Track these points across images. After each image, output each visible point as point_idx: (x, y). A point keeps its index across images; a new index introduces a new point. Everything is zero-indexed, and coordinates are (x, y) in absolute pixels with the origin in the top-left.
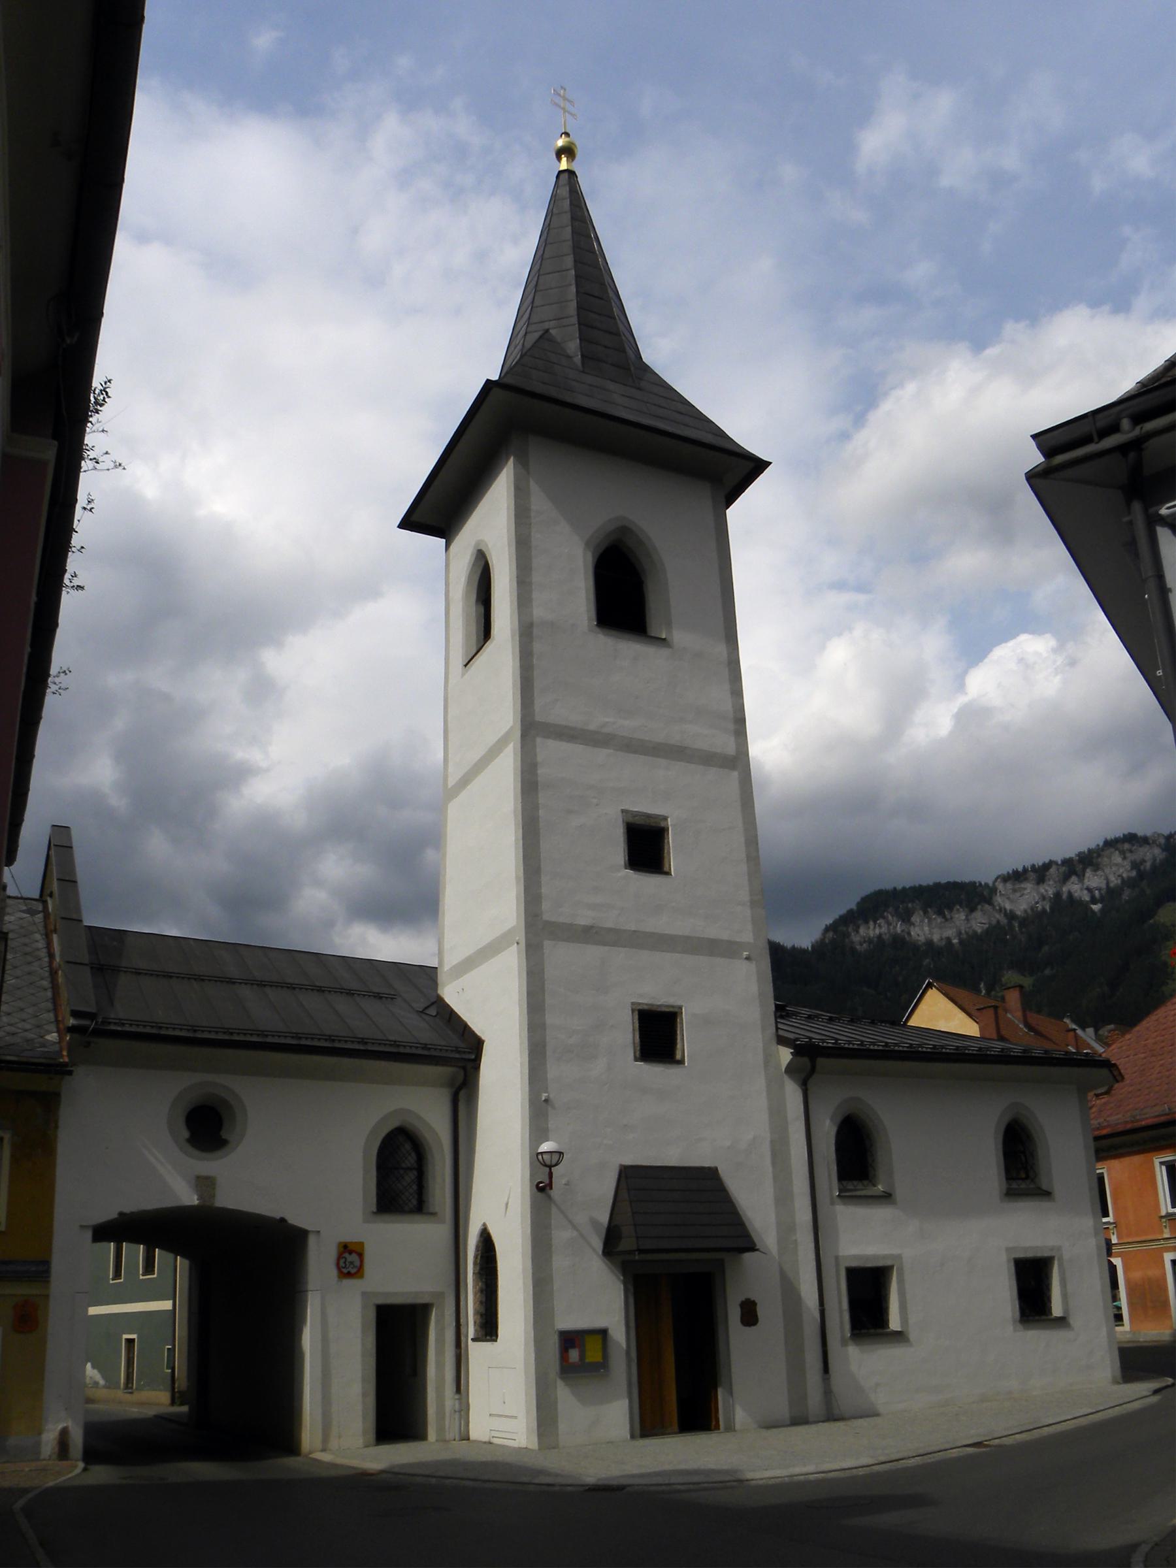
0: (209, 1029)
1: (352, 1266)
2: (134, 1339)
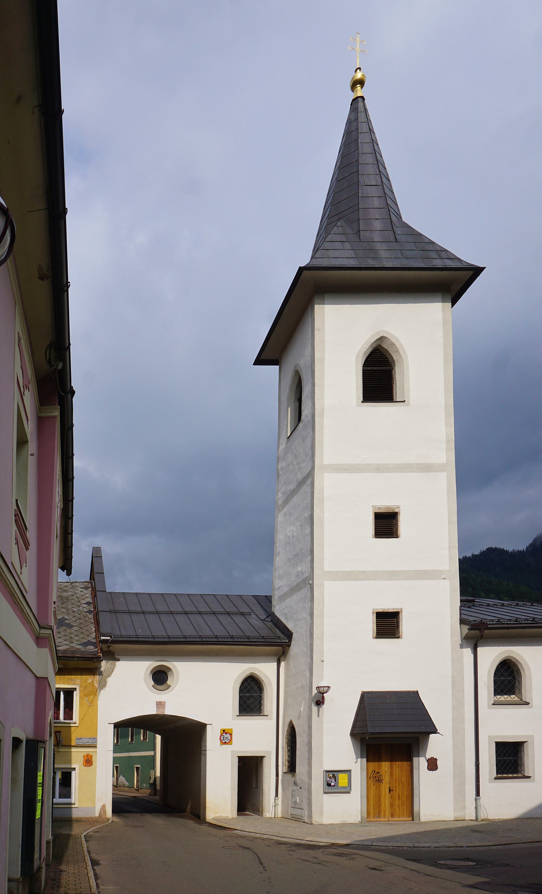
0: (218, 612)
1: (227, 739)
2: (139, 767)
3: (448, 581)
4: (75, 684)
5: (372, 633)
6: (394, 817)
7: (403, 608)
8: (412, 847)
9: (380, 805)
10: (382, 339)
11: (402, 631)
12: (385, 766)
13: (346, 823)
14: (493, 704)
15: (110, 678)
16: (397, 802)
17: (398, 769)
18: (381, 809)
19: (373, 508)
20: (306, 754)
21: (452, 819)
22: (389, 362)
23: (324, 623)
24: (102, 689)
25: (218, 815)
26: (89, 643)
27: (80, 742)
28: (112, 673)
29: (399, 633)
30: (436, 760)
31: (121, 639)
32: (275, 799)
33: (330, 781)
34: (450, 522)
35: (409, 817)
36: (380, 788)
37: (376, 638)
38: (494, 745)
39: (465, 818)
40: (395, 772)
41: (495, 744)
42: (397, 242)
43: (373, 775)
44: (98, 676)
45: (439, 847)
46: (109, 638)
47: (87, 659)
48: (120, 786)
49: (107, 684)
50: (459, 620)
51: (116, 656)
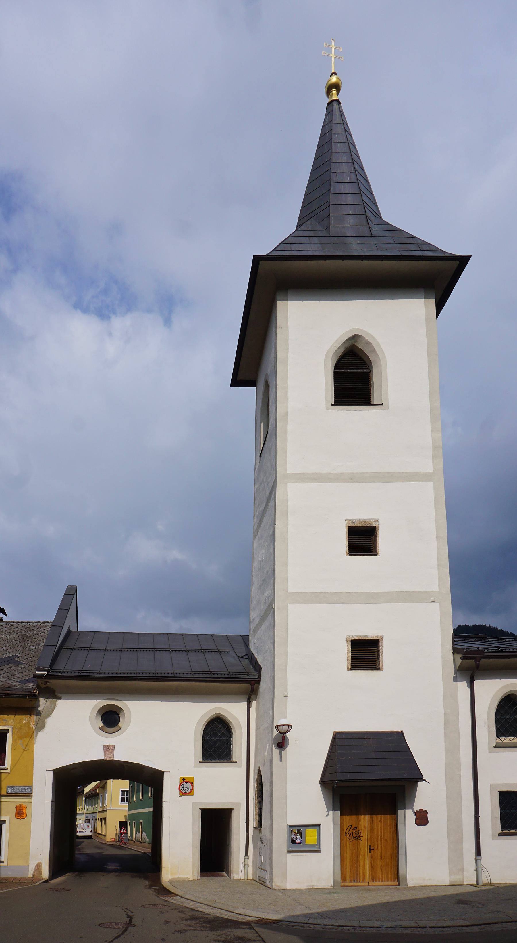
3: (438, 604)
4: (7, 725)
5: (346, 664)
6: (376, 881)
7: (383, 635)
8: (357, 927)
9: (358, 867)
10: (355, 337)
11: (383, 662)
12: (364, 820)
13: (315, 887)
14: (495, 747)
15: (49, 718)
16: (379, 863)
17: (380, 824)
18: (360, 872)
19: (347, 521)
20: (269, 805)
21: (448, 884)
22: (365, 364)
23: (287, 653)
24: (40, 731)
25: (176, 876)
26: (28, 681)
27: (12, 791)
28: (52, 713)
29: (379, 664)
30: (426, 812)
31: (60, 674)
32: (245, 859)
33: (294, 837)
34: (438, 537)
35: (394, 881)
36: (357, 846)
37: (352, 669)
38: (497, 795)
39: (463, 882)
40: (376, 827)
41: (498, 793)
42: (372, 236)
43: (349, 831)
44: (35, 717)
45: (393, 928)
46: (46, 672)
47: (24, 696)
48: (143, 842)
49: (46, 725)
50: (452, 648)
51: (56, 694)
